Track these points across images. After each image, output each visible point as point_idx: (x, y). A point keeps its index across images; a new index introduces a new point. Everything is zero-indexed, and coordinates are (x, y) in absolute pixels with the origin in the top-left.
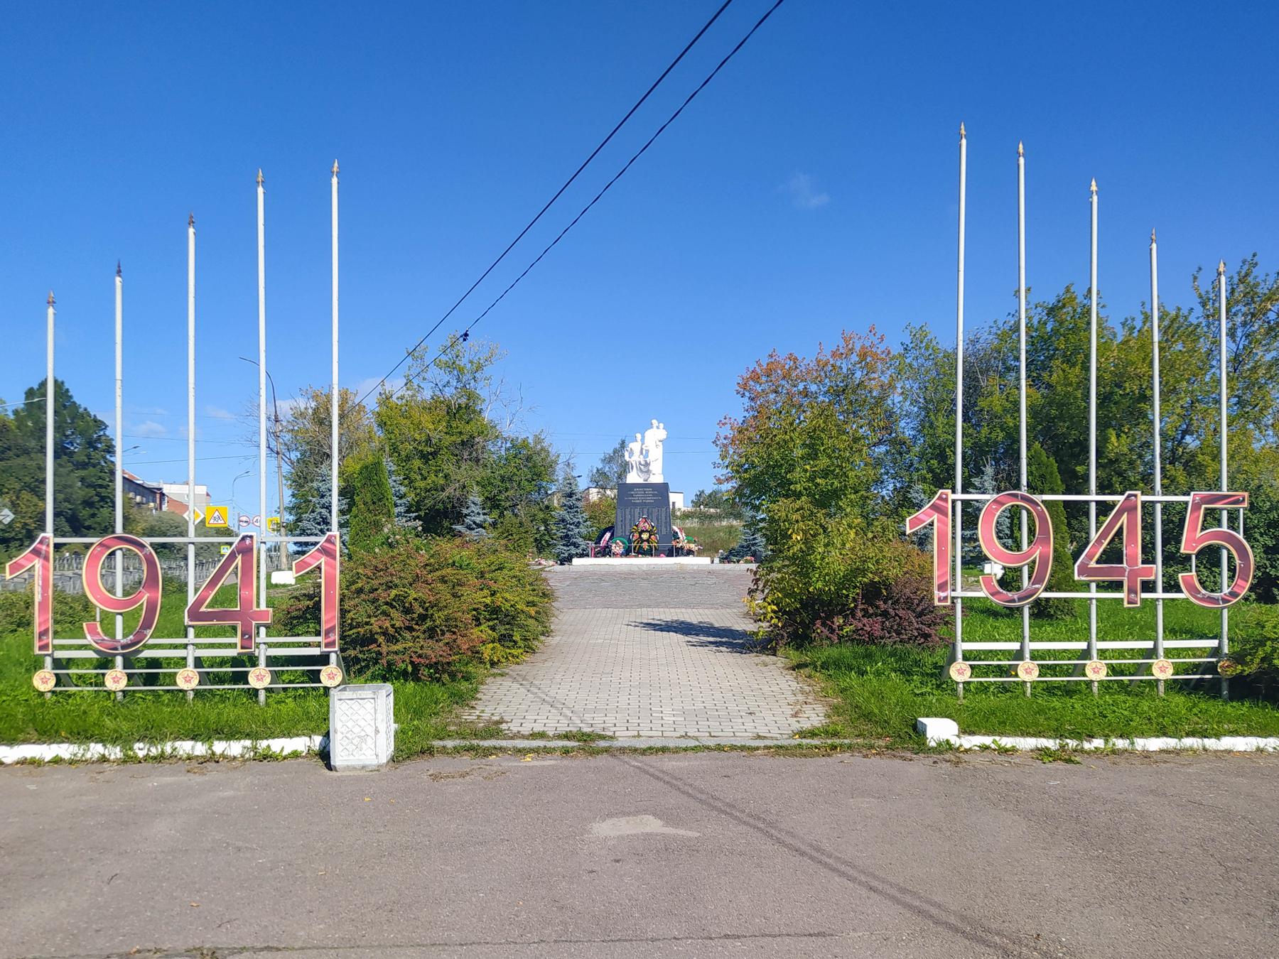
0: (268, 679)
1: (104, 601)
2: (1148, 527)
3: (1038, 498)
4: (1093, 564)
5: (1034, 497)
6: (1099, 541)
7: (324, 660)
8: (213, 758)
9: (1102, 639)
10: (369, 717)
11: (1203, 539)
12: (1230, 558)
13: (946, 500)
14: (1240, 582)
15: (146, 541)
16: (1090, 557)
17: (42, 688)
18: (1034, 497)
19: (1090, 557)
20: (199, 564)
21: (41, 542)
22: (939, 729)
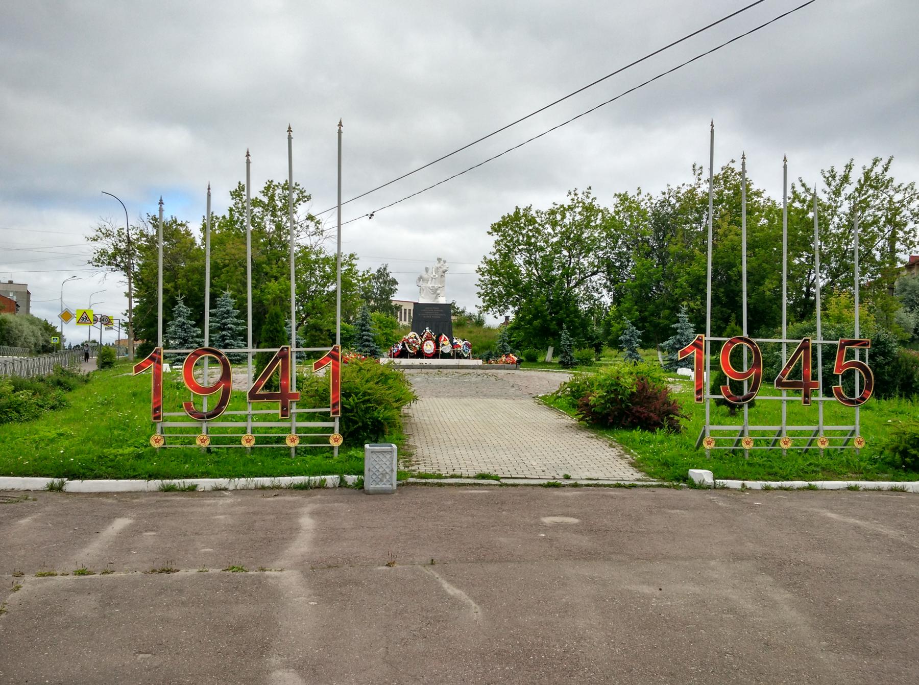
0: (253, 442)
1: (732, 374)
2: (815, 358)
3: (754, 340)
4: (785, 380)
5: (752, 340)
6: (788, 366)
7: (332, 430)
8: (811, 488)
9: (788, 424)
10: (388, 463)
11: (846, 366)
12: (861, 377)
13: (701, 340)
14: (867, 392)
15: (222, 351)
16: (783, 375)
17: (156, 446)
18: (752, 340)
19: (783, 375)
20: (788, 351)
21: (155, 352)
22: (703, 475)
